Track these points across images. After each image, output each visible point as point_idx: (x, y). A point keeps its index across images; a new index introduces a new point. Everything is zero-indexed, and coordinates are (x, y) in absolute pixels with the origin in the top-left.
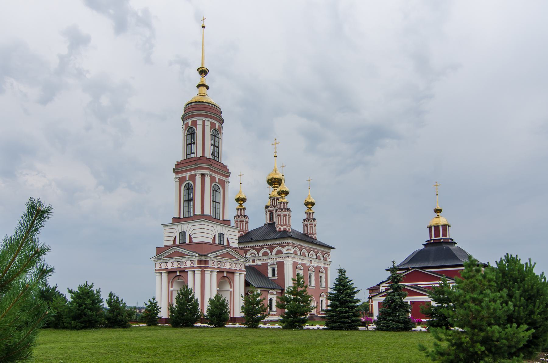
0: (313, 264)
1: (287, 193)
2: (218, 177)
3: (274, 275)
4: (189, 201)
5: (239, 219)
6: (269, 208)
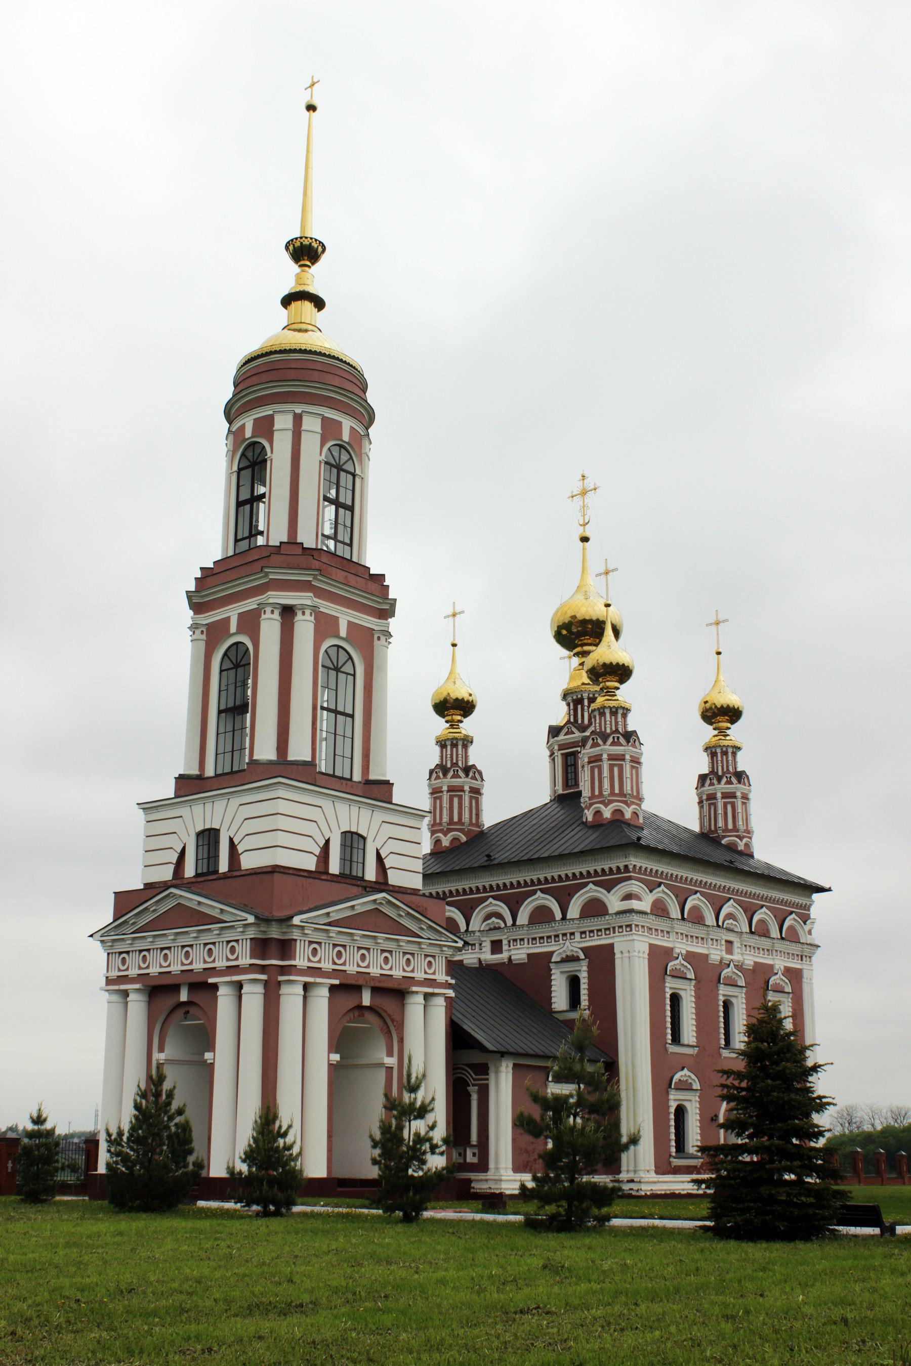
0: (736, 957)
1: (622, 673)
2: (345, 617)
3: (574, 1001)
4: (237, 710)
5: (449, 781)
6: (561, 737)
